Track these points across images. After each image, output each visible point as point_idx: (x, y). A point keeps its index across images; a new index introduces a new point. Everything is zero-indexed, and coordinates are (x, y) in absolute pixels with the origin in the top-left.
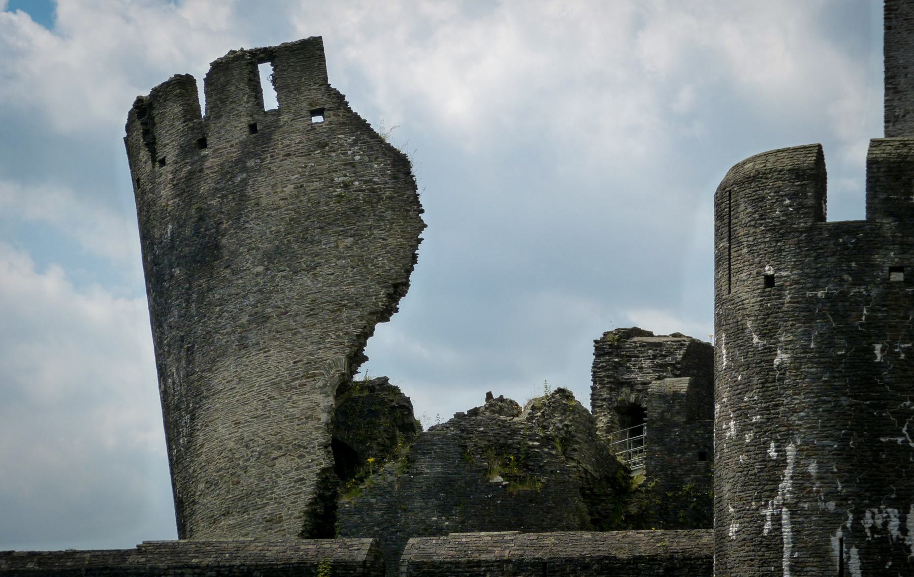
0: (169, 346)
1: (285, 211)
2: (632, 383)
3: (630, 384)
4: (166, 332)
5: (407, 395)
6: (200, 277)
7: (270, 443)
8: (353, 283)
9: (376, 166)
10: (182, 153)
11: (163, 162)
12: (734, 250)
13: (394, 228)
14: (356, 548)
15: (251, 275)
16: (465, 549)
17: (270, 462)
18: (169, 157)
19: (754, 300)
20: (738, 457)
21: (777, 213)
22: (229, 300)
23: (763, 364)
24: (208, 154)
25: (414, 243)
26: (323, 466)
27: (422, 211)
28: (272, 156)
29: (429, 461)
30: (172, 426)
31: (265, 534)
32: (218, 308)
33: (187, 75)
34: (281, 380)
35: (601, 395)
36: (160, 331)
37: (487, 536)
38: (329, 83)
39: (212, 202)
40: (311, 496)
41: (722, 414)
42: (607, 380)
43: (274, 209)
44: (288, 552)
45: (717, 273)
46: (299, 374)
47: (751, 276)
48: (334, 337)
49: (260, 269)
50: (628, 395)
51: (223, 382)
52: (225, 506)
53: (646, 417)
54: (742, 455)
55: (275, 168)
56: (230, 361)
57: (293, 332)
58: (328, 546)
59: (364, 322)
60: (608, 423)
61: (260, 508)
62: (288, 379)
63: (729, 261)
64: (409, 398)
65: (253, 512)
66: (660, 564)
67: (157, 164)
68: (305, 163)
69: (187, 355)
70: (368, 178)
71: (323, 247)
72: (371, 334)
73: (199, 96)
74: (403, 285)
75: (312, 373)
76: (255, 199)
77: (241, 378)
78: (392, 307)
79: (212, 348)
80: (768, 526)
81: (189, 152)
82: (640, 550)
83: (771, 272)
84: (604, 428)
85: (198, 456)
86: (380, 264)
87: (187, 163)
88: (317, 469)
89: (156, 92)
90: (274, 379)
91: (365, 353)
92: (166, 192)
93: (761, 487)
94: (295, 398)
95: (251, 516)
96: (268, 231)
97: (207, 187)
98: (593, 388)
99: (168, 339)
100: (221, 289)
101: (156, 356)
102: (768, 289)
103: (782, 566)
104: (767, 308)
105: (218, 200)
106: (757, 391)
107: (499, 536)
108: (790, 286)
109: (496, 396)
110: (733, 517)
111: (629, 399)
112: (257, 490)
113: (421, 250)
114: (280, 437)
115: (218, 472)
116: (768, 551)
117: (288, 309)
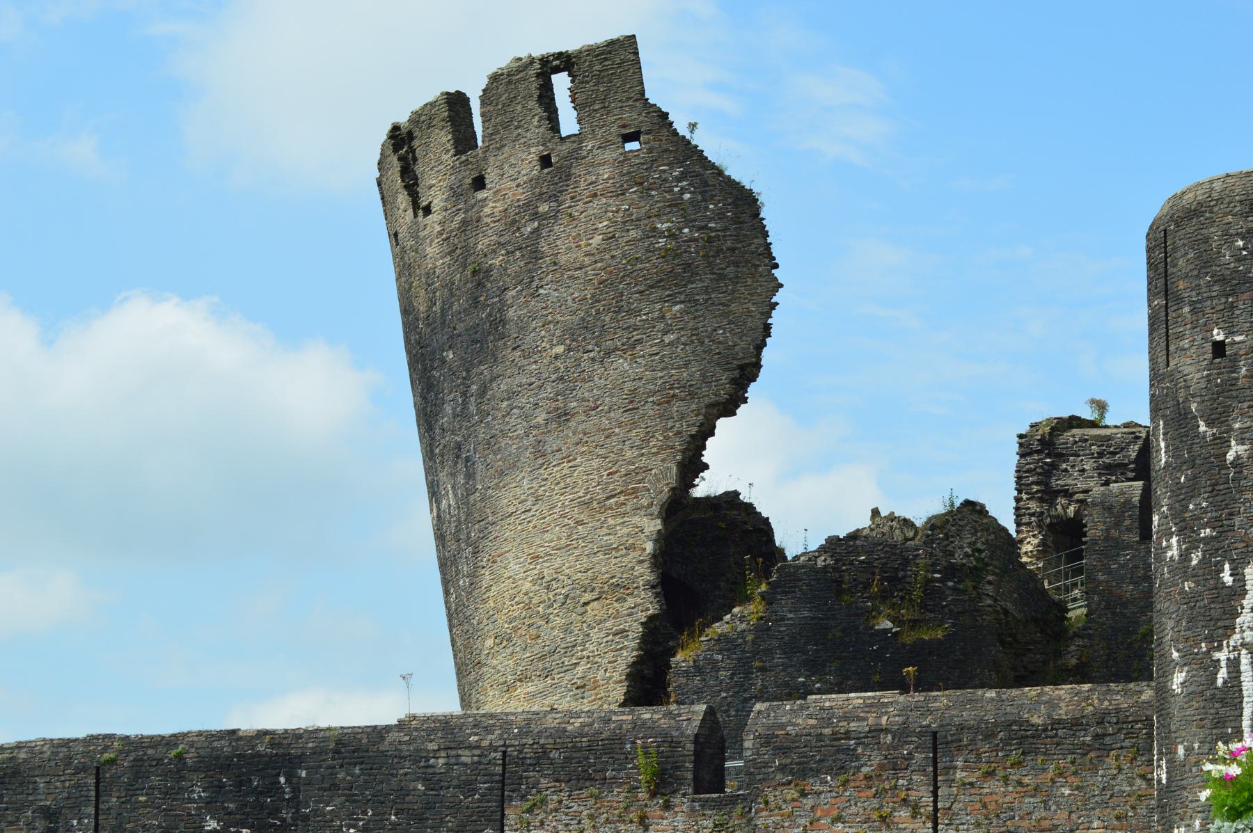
0: (442, 456)
1: (592, 270)
2: (1071, 491)
3: (1067, 493)
4: (437, 438)
5: (765, 515)
6: (480, 363)
7: (578, 583)
8: (686, 366)
9: (711, 206)
10: (453, 196)
11: (427, 210)
12: (1173, 309)
13: (738, 290)
14: (685, 718)
15: (548, 358)
16: (829, 716)
17: (580, 610)
18: (435, 202)
19: (1198, 375)
20: (1183, 584)
21: (1227, 257)
22: (520, 392)
23: (1212, 459)
24: (487, 197)
25: (766, 309)
26: (650, 612)
27: (776, 266)
28: (572, 198)
29: (792, 603)
30: (449, 564)
31: (575, 704)
32: (506, 403)
33: (457, 91)
34: (592, 498)
35: (1029, 508)
36: (430, 436)
37: (858, 698)
38: (646, 97)
39: (494, 261)
40: (635, 653)
41: (1162, 528)
42: (1035, 488)
43: (576, 269)
44: (596, 725)
45: (1151, 341)
46: (614, 490)
47: (1196, 343)
48: (661, 438)
49: (560, 349)
50: (1065, 508)
51: (514, 502)
52: (521, 668)
53: (1086, 536)
54: (1187, 581)
55: (576, 214)
56: (523, 474)
57: (606, 433)
58: (647, 716)
59: (701, 417)
60: (1038, 546)
61: (568, 670)
62: (601, 496)
63: (1167, 324)
64: (768, 519)
65: (559, 676)
66: (1085, 730)
67: (421, 213)
68: (617, 205)
69: (466, 466)
70: (703, 224)
71: (644, 317)
72: (712, 434)
73: (475, 121)
74: (753, 367)
75: (633, 489)
76: (550, 256)
77: (537, 496)
78: (738, 397)
79: (498, 457)
80: (1222, 674)
81: (462, 195)
82: (1060, 712)
83: (1220, 338)
84: (1035, 553)
85: (485, 601)
86: (721, 339)
87: (460, 210)
88: (642, 617)
89: (416, 118)
90: (581, 497)
91: (704, 459)
92: (432, 250)
93: (1212, 623)
94: (611, 521)
95: (556, 681)
96: (569, 298)
97: (486, 241)
98: (1018, 500)
99: (441, 447)
100: (509, 377)
101: (425, 469)
102: (1217, 360)
103: (1241, 727)
104: (1217, 385)
105: (501, 258)
106: (1206, 495)
107: (874, 698)
108: (1245, 354)
109: (884, 513)
110: (1177, 664)
111: (1065, 512)
112: (563, 646)
113: (776, 319)
114: (592, 574)
115: (510, 623)
116: (1222, 707)
117: (599, 403)
